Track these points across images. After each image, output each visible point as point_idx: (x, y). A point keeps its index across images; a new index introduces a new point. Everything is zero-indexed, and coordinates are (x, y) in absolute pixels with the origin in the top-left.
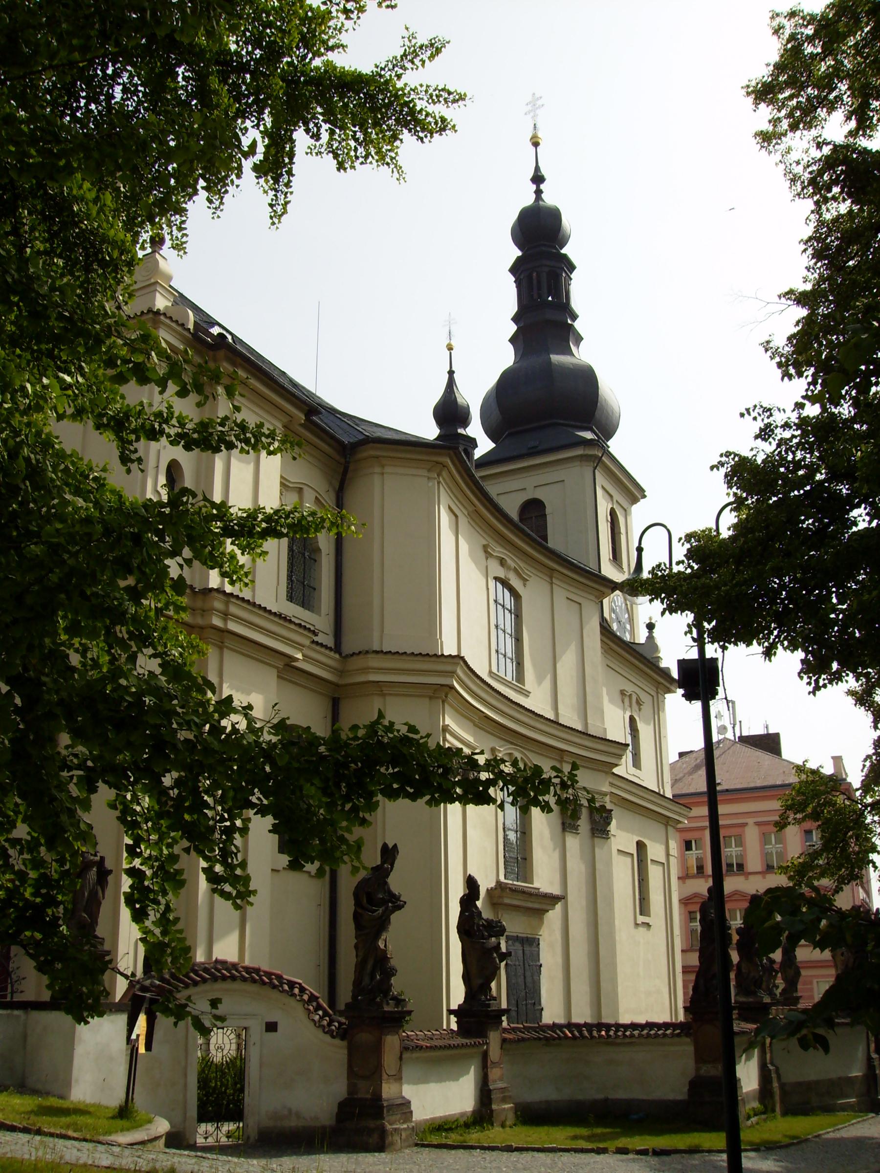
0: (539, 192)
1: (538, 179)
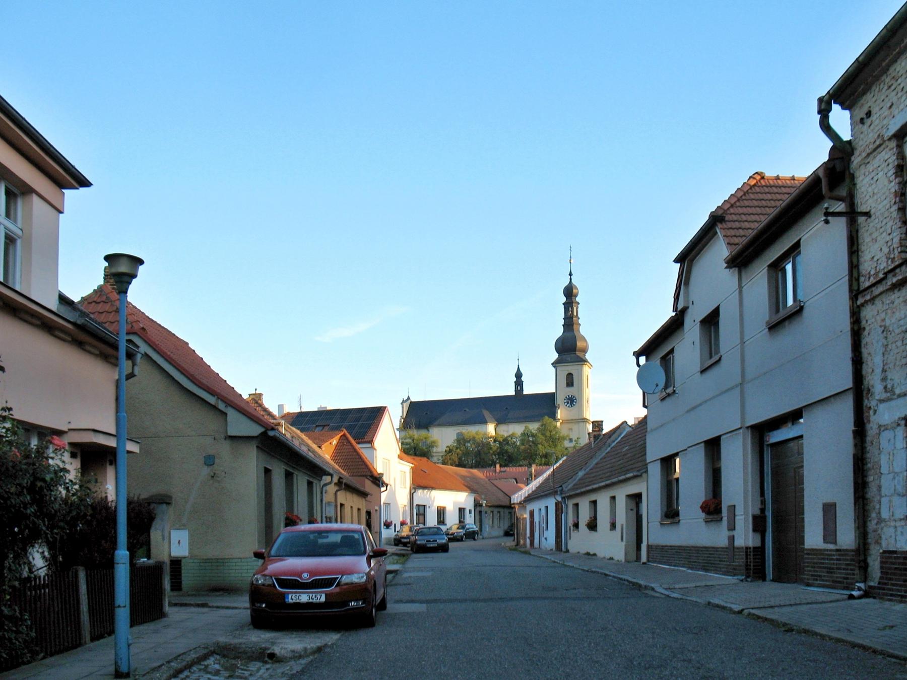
1: (571, 275)
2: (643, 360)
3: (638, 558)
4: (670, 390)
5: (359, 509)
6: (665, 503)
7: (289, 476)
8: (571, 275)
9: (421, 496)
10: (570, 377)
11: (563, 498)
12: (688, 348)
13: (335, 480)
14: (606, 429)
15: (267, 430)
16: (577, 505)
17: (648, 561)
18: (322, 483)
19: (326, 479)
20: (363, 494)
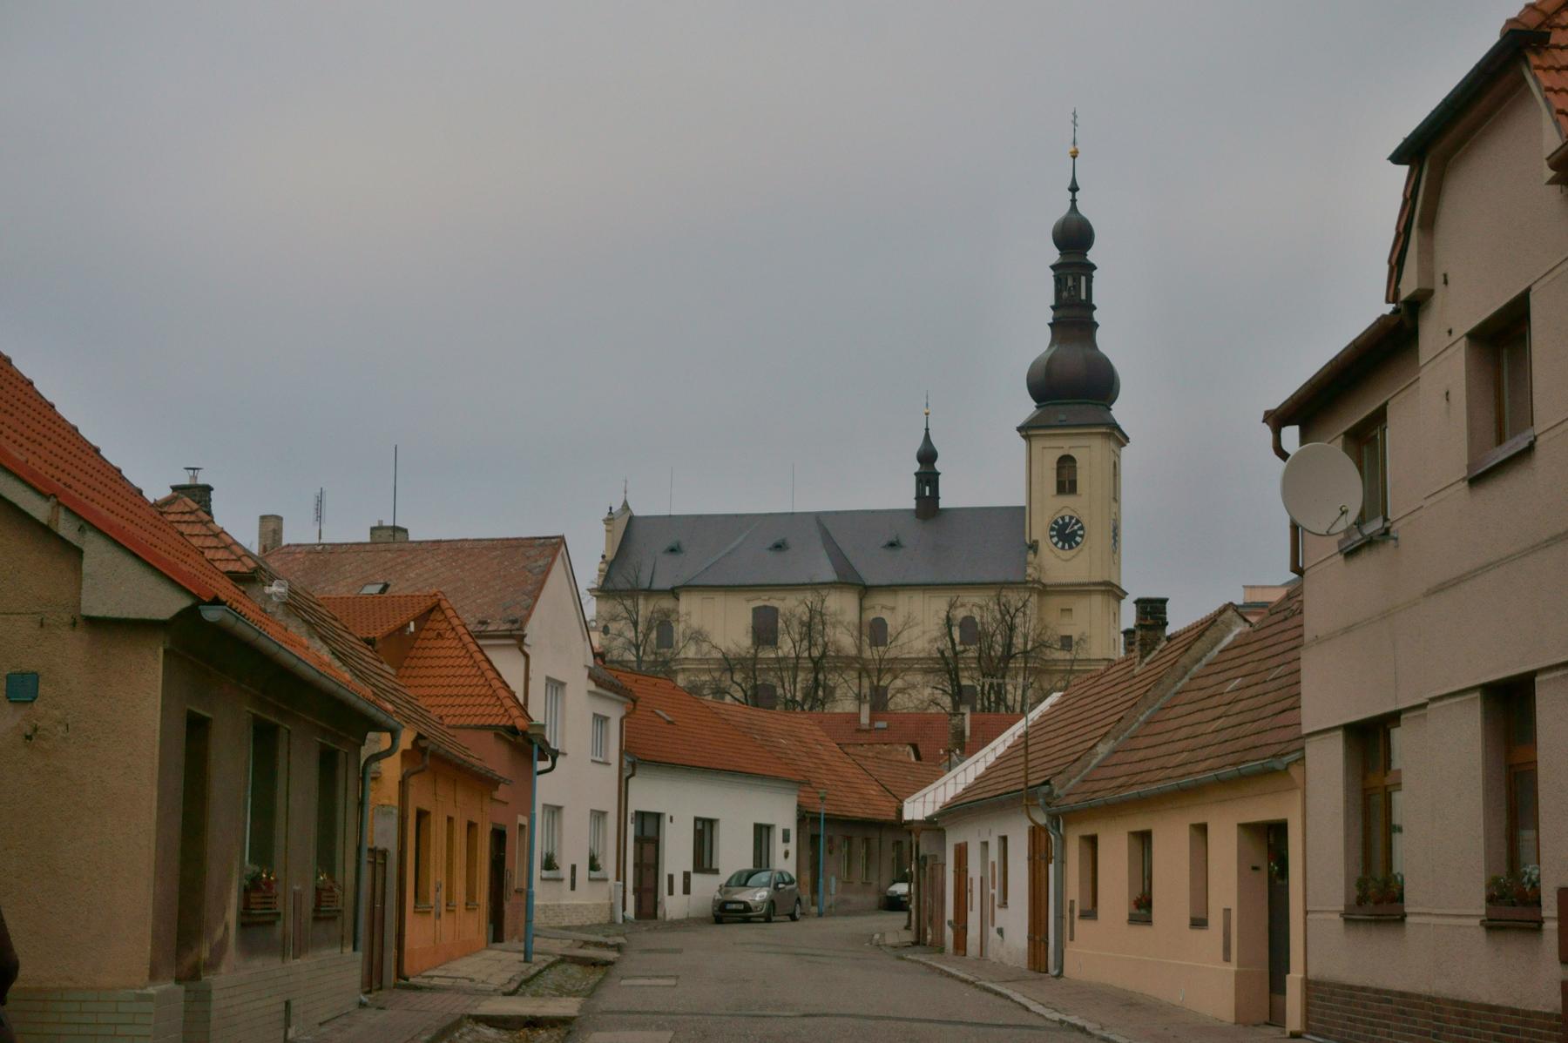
1: (1074, 189)
2: (1291, 435)
3: (1276, 1017)
4: (1374, 526)
5: (471, 826)
6: (1358, 853)
7: (265, 738)
8: (1074, 189)
9: (649, 794)
10: (1066, 464)
11: (1054, 818)
12: (1432, 409)
13: (406, 740)
14: (1178, 620)
15: (199, 601)
16: (1092, 841)
17: (1308, 1029)
18: (365, 752)
19: (381, 741)
20: (484, 783)
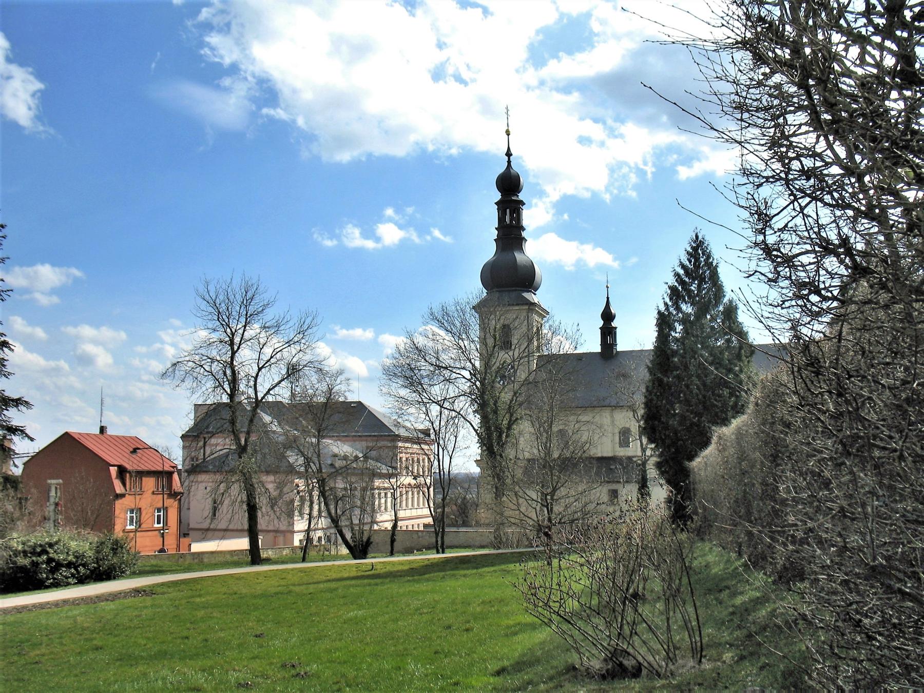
0: (509, 162)
